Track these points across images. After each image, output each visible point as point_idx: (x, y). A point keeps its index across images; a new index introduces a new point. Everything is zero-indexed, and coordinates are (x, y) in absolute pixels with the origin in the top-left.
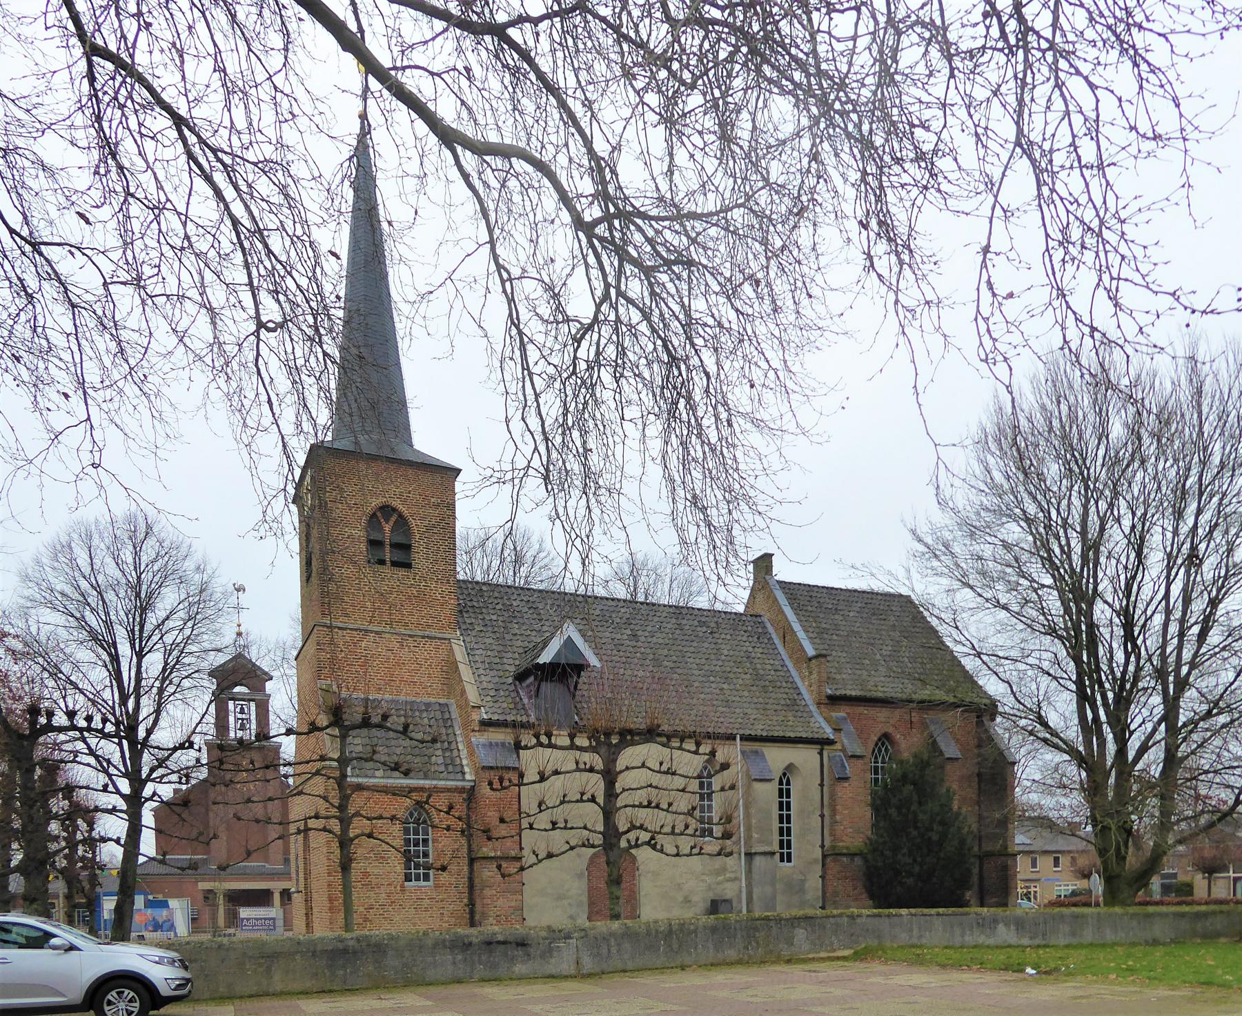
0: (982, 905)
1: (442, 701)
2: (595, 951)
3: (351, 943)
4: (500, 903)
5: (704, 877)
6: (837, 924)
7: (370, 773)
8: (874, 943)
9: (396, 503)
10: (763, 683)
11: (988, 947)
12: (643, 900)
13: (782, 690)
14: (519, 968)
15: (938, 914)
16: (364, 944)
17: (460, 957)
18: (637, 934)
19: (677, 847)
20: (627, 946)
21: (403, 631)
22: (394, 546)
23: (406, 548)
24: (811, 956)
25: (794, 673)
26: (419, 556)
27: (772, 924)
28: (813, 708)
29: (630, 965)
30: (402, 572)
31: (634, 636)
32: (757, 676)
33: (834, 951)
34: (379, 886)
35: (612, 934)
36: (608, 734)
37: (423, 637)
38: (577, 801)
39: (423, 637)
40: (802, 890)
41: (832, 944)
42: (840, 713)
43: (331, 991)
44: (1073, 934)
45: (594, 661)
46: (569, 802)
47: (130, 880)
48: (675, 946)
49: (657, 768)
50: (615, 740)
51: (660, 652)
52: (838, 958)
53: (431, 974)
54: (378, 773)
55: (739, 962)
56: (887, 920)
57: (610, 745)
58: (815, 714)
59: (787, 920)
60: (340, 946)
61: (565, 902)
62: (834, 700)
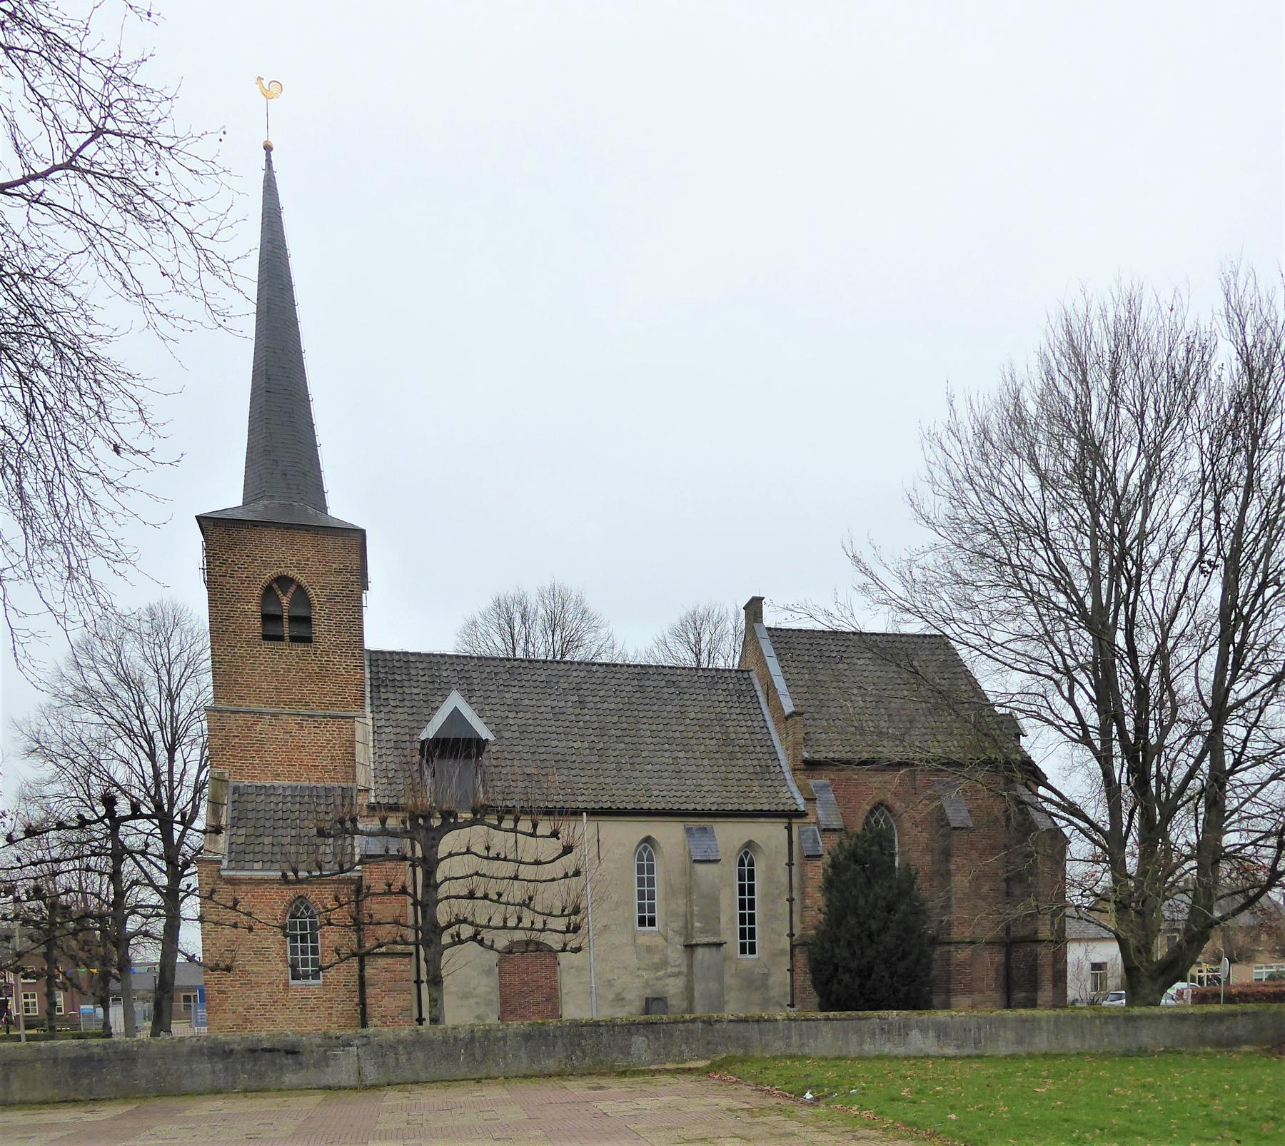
0: (1008, 1006)
1: (344, 785)
2: (380, 1060)
3: (96, 1050)
4: (386, 1002)
5: (640, 973)
6: (688, 1031)
7: (247, 865)
8: (740, 1052)
9: (293, 573)
10: (730, 749)
11: (896, 1057)
12: (565, 998)
13: (754, 756)
14: (289, 1078)
15: (827, 1019)
16: (110, 1051)
17: (220, 1066)
18: (432, 1041)
19: (493, 941)
20: (419, 1055)
21: (303, 711)
22: (293, 619)
23: (307, 620)
24: (653, 1067)
25: (774, 736)
26: (321, 629)
27: (602, 1030)
28: (788, 776)
29: (423, 1076)
30: (301, 647)
31: (582, 703)
32: (727, 741)
33: (685, 1061)
34: (259, 985)
35: (400, 1042)
36: (427, 817)
37: (325, 717)
38: (385, 894)
39: (325, 717)
40: (764, 986)
41: (681, 1053)
42: (818, 781)
43: (74, 1101)
44: (1020, 1042)
45: (485, 733)
46: (374, 894)
47: (167, 974)
48: (479, 1055)
49: (484, 853)
50: (436, 823)
51: (609, 719)
52: (689, 1070)
53: (187, 1083)
54: (257, 866)
55: (560, 1075)
56: (756, 1026)
57: (429, 829)
58: (790, 783)
59: (622, 1026)
60: (84, 1053)
61: (472, 1001)
62: (812, 766)
